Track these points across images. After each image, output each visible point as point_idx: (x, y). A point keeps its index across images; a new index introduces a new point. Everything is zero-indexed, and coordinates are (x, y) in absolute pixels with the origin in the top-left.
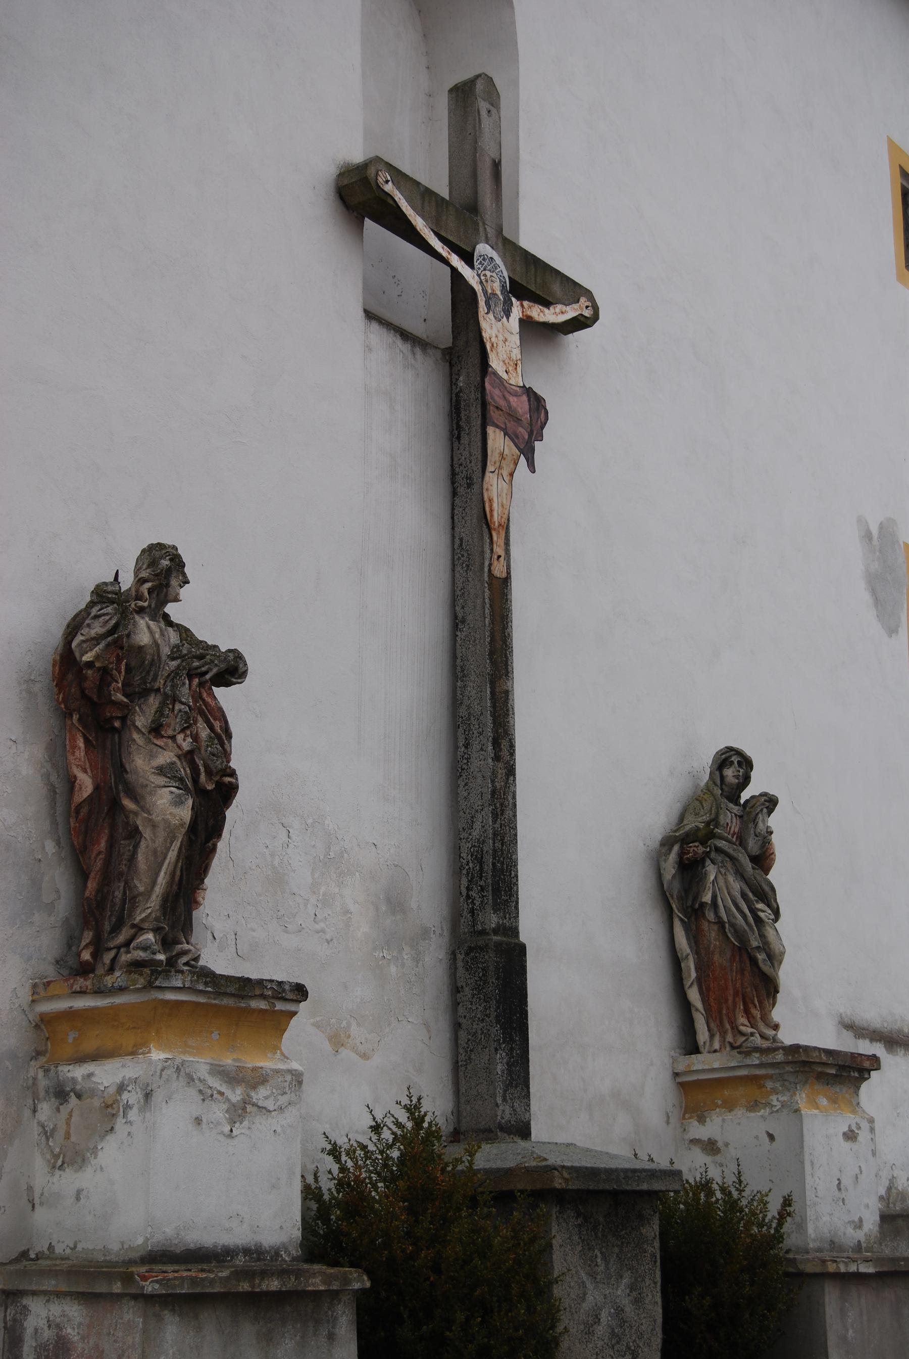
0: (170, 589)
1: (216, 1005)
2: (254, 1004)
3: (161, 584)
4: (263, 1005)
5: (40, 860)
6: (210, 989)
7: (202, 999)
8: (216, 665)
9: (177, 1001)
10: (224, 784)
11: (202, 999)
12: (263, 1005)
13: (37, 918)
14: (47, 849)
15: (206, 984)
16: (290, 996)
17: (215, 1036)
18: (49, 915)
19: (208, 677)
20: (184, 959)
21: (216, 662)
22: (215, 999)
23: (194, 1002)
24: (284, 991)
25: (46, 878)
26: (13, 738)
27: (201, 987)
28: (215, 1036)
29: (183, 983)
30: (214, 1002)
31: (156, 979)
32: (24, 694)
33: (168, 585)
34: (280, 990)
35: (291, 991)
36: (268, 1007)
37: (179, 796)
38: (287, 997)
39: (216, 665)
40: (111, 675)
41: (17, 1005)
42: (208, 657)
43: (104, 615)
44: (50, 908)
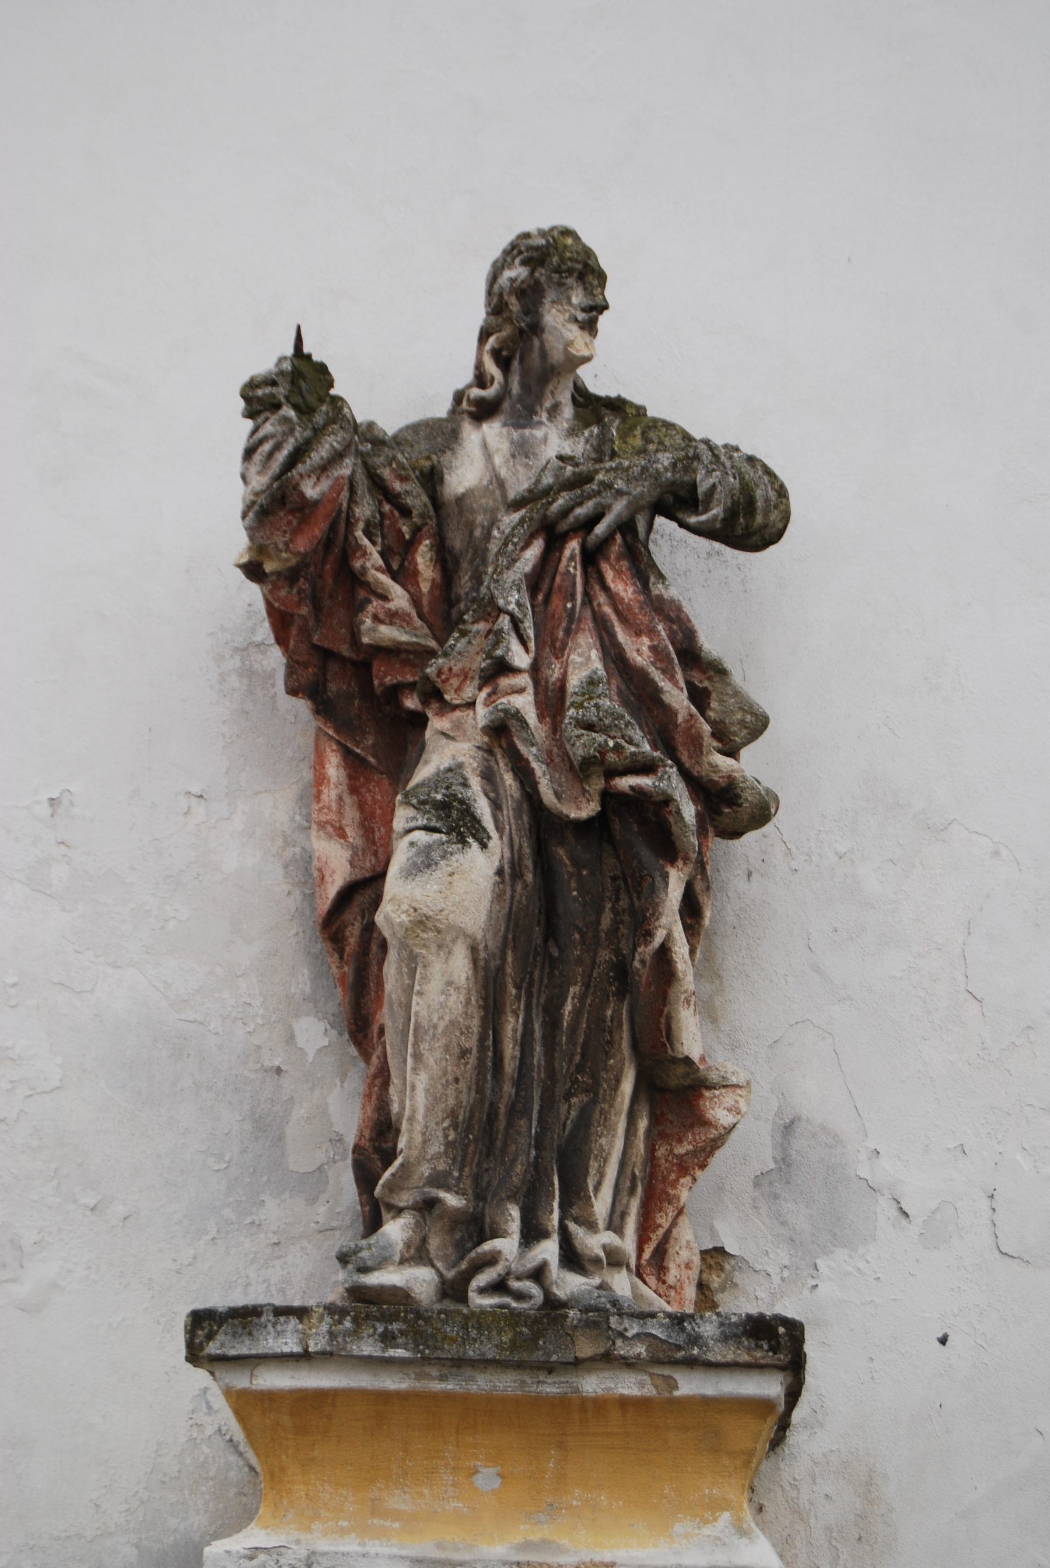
0: (546, 336)
1: (448, 1396)
2: (592, 1384)
3: (521, 331)
4: (629, 1385)
5: (279, 1071)
6: (400, 1353)
7: (392, 1382)
8: (620, 493)
9: (300, 1391)
10: (621, 796)
11: (392, 1382)
12: (629, 1385)
13: (273, 1211)
14: (301, 1040)
15: (388, 1339)
16: (719, 1353)
17: (487, 1479)
18: (312, 1201)
19: (600, 529)
20: (483, 1279)
21: (620, 484)
22: (443, 1378)
23: (363, 1393)
24: (695, 1340)
25: (300, 1112)
26: (196, 790)
27: (368, 1348)
28: (487, 1479)
29: (303, 1342)
30: (450, 1386)
31: (210, 1337)
32: (234, 681)
33: (536, 328)
34: (681, 1340)
35: (725, 1338)
36: (649, 1391)
37: (428, 848)
38: (711, 1357)
39: (620, 493)
40: (366, 585)
41: (210, 1431)
42: (600, 477)
43: (261, 442)
44: (312, 1184)
